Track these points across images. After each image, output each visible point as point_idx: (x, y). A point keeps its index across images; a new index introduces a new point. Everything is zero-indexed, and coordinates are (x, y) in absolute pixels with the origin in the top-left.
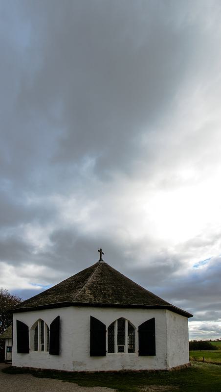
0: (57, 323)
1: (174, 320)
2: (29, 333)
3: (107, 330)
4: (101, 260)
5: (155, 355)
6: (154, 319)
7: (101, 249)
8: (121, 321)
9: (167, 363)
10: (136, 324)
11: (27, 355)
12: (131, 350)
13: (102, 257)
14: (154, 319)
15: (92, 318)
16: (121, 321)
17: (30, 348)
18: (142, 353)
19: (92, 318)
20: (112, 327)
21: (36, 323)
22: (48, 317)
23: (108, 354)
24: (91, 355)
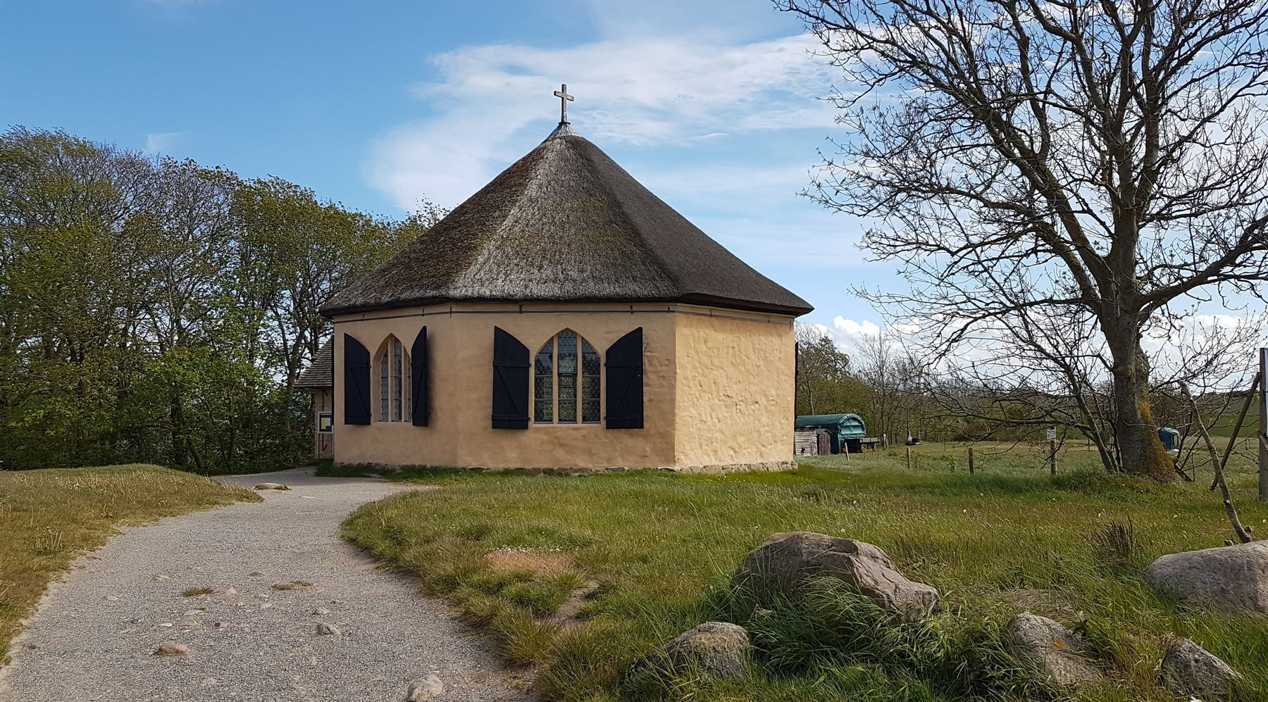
0: (423, 343)
1: (485, 428)
2: (371, 370)
3: (532, 362)
5: (642, 427)
6: (640, 329)
8: (567, 336)
9: (404, 571)
10: (601, 346)
11: (368, 430)
12: (592, 416)
14: (640, 329)
15: (498, 331)
16: (567, 336)
17: (372, 412)
18: (615, 422)
19: (498, 331)
20: (546, 350)
21: (384, 344)
22: (406, 329)
23: (532, 424)
24: (494, 427)
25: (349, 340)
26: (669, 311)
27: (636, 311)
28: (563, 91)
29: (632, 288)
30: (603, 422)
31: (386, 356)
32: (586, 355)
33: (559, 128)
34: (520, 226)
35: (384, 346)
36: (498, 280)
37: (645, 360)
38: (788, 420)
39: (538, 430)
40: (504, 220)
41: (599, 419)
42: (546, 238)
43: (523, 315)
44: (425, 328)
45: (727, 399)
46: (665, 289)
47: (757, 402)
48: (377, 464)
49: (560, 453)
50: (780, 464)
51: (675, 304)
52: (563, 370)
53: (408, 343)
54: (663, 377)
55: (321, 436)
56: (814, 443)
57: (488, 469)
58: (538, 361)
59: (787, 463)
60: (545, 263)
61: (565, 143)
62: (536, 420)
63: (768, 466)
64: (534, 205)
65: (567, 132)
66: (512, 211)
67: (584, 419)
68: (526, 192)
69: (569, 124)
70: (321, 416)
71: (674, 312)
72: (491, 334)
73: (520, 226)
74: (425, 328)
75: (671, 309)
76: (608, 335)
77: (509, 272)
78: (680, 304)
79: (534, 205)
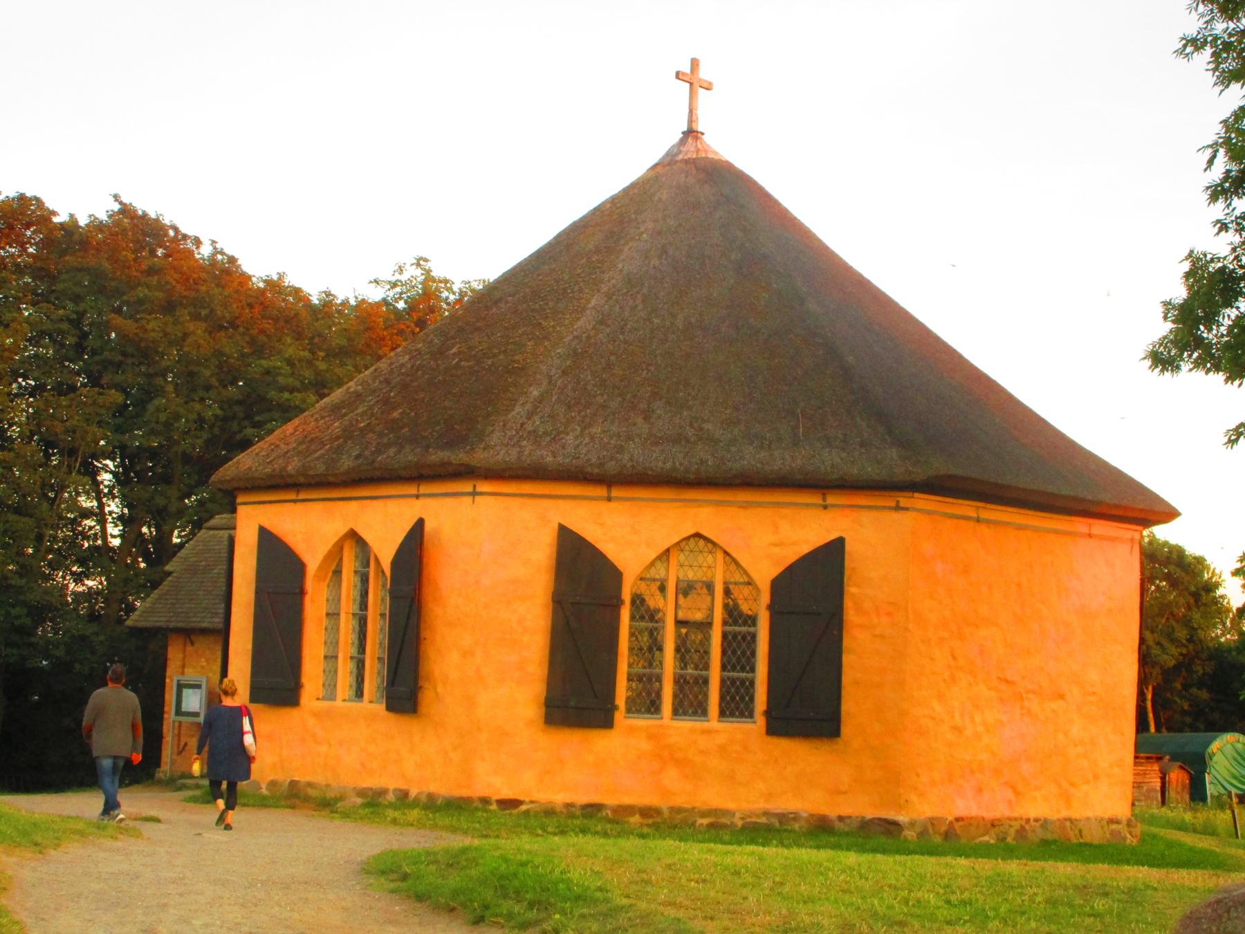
3: (626, 596)
4: (691, 133)
6: (419, 526)
7: (695, 63)
10: (764, 572)
13: (701, 112)
21: (338, 549)
23: (619, 716)
25: (270, 543)
26: (898, 508)
27: (833, 506)
28: (692, 71)
29: (829, 460)
30: (760, 721)
31: (338, 572)
32: (731, 587)
33: (683, 142)
34: (608, 330)
35: (336, 554)
36: (568, 434)
37: (848, 603)
38: (1123, 734)
39: (632, 730)
40: (578, 319)
41: (751, 715)
42: (659, 358)
43: (613, 505)
44: (420, 523)
45: (1003, 687)
46: (893, 461)
47: (1062, 697)
48: (310, 785)
49: (672, 778)
50: (1104, 823)
51: (910, 494)
52: (681, 615)
53: (385, 548)
54: (882, 637)
55: (177, 724)
56: (1155, 790)
57: (532, 802)
58: (638, 600)
59: (1118, 822)
60: (657, 404)
61: (694, 172)
62: (629, 711)
63: (1080, 825)
64: (635, 290)
65: (698, 151)
66: (593, 302)
67: (677, 712)
68: (620, 266)
69: (703, 134)
70: (180, 687)
71: (906, 509)
72: (257, 527)
73: (608, 330)
74: (420, 523)
75: (902, 504)
76: (776, 550)
77: (587, 420)
78: (922, 496)
79: (635, 290)
